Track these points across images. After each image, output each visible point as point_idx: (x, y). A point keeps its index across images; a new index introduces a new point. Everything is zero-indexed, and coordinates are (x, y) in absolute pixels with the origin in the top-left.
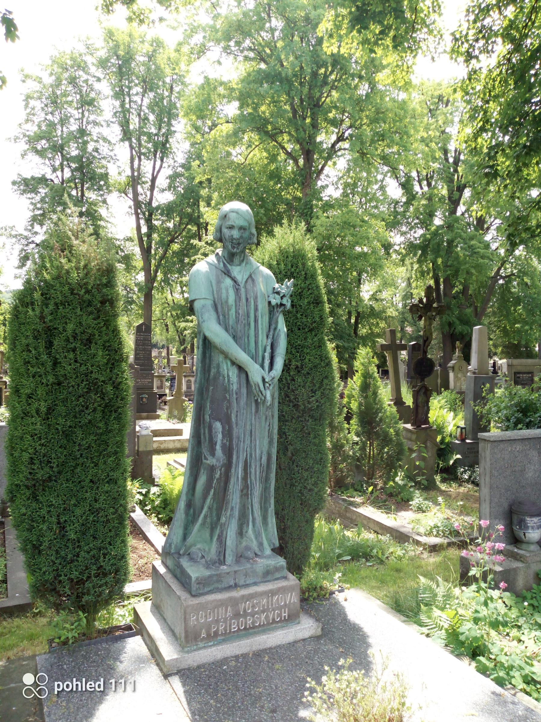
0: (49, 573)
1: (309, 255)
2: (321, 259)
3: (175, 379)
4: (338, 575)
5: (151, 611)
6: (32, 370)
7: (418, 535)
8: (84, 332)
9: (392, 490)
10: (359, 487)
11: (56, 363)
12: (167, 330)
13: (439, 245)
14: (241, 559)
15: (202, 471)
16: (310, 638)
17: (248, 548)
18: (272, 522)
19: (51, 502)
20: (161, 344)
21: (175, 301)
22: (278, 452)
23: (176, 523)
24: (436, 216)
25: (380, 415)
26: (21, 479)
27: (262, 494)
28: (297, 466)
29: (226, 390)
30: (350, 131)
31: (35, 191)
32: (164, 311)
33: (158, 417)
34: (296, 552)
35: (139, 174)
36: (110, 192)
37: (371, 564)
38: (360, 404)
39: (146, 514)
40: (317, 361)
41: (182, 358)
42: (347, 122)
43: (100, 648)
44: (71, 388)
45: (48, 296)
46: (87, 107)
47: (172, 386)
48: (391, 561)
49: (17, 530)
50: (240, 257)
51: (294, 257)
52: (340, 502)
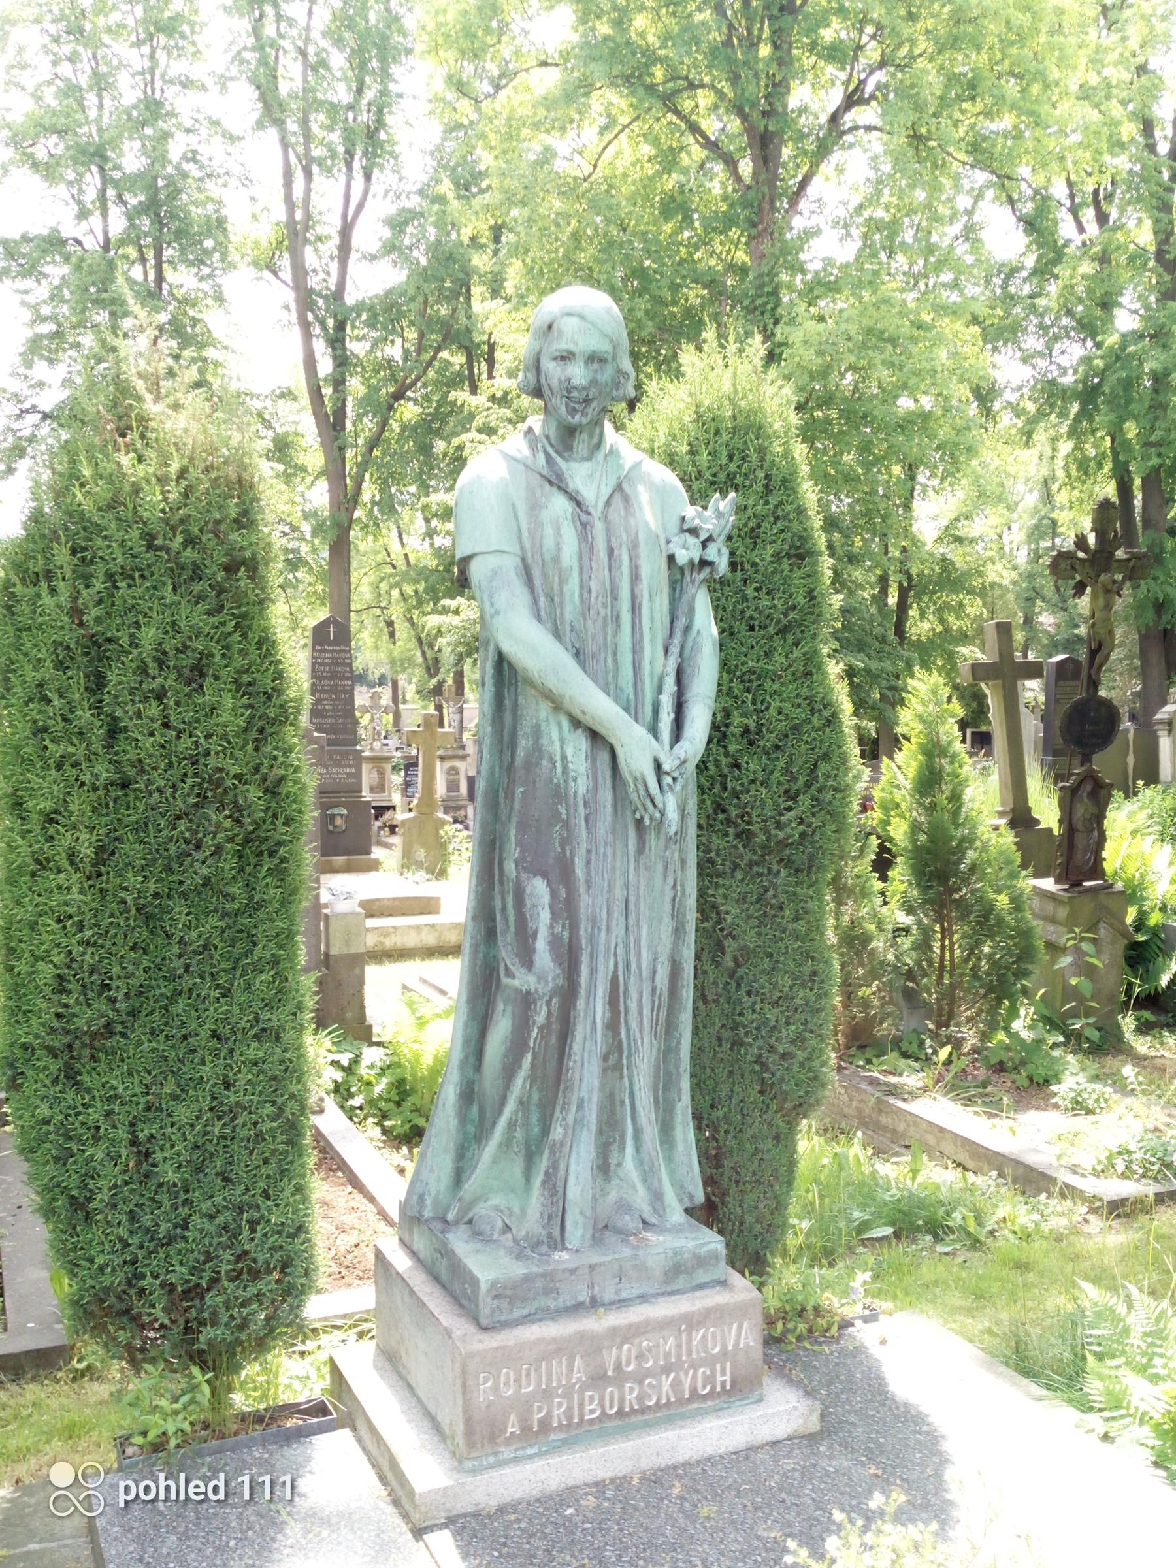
0: (114, 1270)
1: (777, 426)
2: (808, 433)
3: (416, 765)
4: (862, 1277)
5: (375, 1367)
6: (56, 750)
7: (1075, 1173)
8: (184, 649)
9: (1004, 1056)
10: (914, 1048)
11: (114, 731)
12: (392, 635)
13: (1128, 384)
14: (607, 1233)
15: (500, 1006)
16: (790, 1438)
17: (624, 1206)
18: (685, 1140)
19: (113, 1088)
20: (377, 676)
21: (412, 560)
22: (698, 957)
23: (434, 1141)
24: (1120, 305)
25: (970, 854)
26: (35, 1030)
27: (657, 1067)
28: (749, 994)
29: (559, 795)
30: (880, 76)
31: (31, 270)
32: (384, 586)
33: (374, 866)
34: (749, 1219)
35: (308, 216)
36: (230, 266)
37: (948, 1249)
38: (915, 828)
39: (351, 1119)
40: (801, 714)
41: (431, 710)
42: (873, 52)
43: (249, 1459)
44: (156, 795)
45: (88, 555)
46: (163, 39)
47: (407, 785)
48: (1001, 1243)
49: (27, 1160)
50: (591, 436)
51: (734, 431)
52: (864, 1086)
